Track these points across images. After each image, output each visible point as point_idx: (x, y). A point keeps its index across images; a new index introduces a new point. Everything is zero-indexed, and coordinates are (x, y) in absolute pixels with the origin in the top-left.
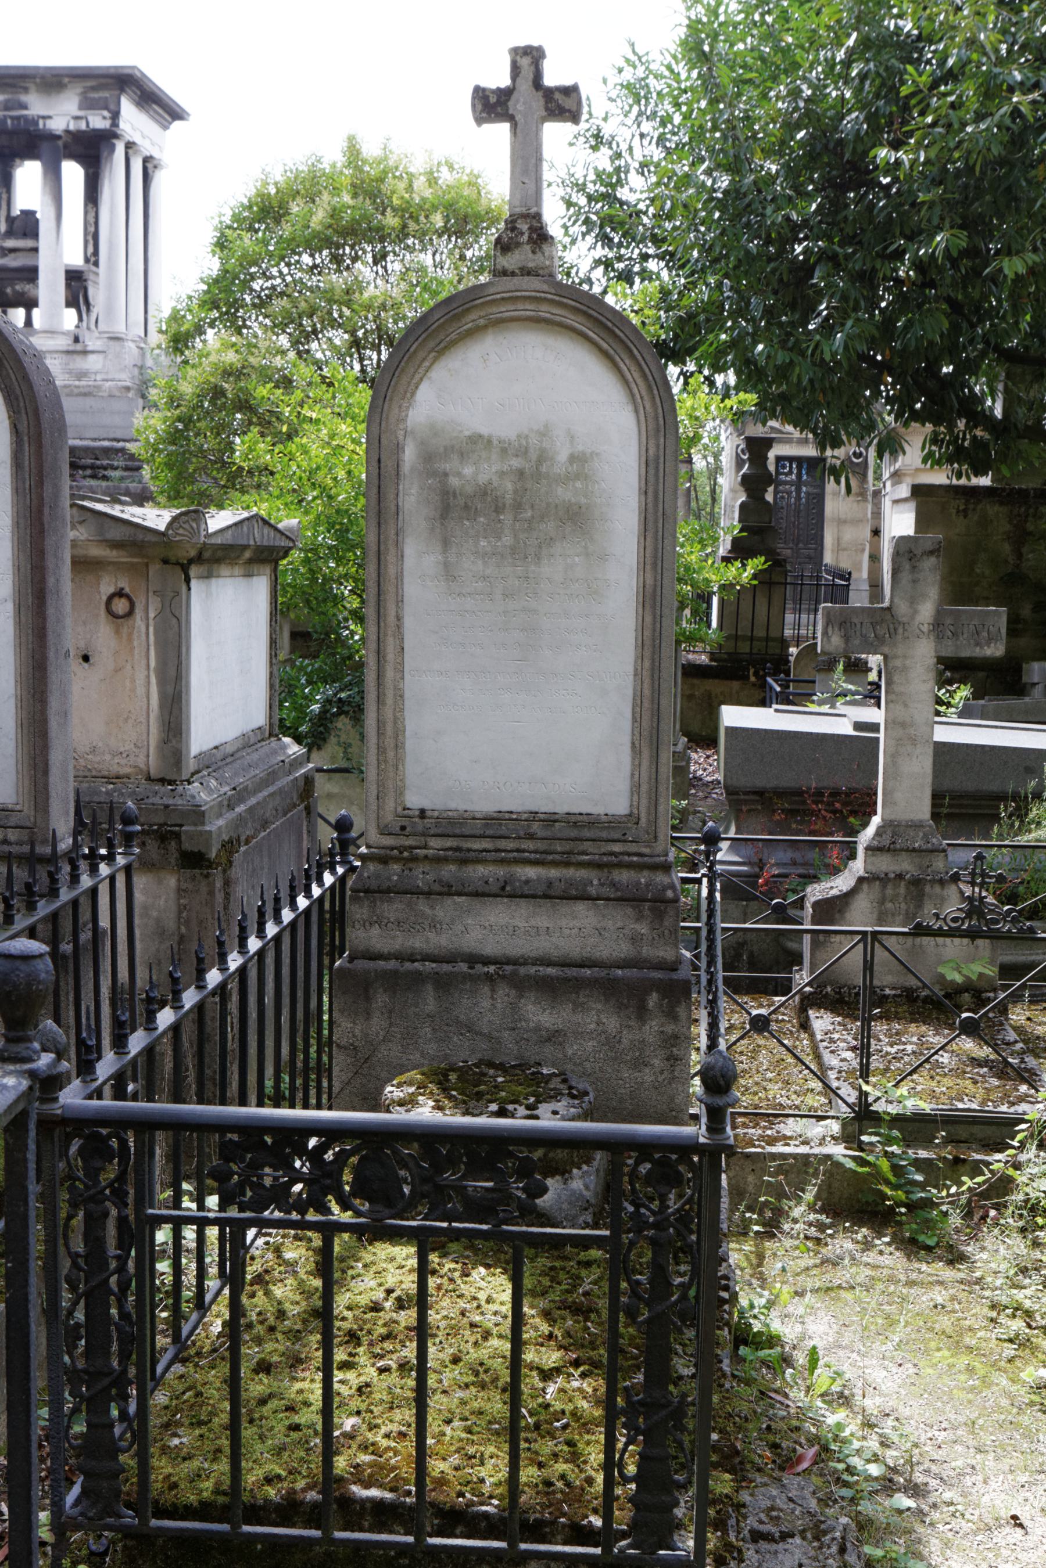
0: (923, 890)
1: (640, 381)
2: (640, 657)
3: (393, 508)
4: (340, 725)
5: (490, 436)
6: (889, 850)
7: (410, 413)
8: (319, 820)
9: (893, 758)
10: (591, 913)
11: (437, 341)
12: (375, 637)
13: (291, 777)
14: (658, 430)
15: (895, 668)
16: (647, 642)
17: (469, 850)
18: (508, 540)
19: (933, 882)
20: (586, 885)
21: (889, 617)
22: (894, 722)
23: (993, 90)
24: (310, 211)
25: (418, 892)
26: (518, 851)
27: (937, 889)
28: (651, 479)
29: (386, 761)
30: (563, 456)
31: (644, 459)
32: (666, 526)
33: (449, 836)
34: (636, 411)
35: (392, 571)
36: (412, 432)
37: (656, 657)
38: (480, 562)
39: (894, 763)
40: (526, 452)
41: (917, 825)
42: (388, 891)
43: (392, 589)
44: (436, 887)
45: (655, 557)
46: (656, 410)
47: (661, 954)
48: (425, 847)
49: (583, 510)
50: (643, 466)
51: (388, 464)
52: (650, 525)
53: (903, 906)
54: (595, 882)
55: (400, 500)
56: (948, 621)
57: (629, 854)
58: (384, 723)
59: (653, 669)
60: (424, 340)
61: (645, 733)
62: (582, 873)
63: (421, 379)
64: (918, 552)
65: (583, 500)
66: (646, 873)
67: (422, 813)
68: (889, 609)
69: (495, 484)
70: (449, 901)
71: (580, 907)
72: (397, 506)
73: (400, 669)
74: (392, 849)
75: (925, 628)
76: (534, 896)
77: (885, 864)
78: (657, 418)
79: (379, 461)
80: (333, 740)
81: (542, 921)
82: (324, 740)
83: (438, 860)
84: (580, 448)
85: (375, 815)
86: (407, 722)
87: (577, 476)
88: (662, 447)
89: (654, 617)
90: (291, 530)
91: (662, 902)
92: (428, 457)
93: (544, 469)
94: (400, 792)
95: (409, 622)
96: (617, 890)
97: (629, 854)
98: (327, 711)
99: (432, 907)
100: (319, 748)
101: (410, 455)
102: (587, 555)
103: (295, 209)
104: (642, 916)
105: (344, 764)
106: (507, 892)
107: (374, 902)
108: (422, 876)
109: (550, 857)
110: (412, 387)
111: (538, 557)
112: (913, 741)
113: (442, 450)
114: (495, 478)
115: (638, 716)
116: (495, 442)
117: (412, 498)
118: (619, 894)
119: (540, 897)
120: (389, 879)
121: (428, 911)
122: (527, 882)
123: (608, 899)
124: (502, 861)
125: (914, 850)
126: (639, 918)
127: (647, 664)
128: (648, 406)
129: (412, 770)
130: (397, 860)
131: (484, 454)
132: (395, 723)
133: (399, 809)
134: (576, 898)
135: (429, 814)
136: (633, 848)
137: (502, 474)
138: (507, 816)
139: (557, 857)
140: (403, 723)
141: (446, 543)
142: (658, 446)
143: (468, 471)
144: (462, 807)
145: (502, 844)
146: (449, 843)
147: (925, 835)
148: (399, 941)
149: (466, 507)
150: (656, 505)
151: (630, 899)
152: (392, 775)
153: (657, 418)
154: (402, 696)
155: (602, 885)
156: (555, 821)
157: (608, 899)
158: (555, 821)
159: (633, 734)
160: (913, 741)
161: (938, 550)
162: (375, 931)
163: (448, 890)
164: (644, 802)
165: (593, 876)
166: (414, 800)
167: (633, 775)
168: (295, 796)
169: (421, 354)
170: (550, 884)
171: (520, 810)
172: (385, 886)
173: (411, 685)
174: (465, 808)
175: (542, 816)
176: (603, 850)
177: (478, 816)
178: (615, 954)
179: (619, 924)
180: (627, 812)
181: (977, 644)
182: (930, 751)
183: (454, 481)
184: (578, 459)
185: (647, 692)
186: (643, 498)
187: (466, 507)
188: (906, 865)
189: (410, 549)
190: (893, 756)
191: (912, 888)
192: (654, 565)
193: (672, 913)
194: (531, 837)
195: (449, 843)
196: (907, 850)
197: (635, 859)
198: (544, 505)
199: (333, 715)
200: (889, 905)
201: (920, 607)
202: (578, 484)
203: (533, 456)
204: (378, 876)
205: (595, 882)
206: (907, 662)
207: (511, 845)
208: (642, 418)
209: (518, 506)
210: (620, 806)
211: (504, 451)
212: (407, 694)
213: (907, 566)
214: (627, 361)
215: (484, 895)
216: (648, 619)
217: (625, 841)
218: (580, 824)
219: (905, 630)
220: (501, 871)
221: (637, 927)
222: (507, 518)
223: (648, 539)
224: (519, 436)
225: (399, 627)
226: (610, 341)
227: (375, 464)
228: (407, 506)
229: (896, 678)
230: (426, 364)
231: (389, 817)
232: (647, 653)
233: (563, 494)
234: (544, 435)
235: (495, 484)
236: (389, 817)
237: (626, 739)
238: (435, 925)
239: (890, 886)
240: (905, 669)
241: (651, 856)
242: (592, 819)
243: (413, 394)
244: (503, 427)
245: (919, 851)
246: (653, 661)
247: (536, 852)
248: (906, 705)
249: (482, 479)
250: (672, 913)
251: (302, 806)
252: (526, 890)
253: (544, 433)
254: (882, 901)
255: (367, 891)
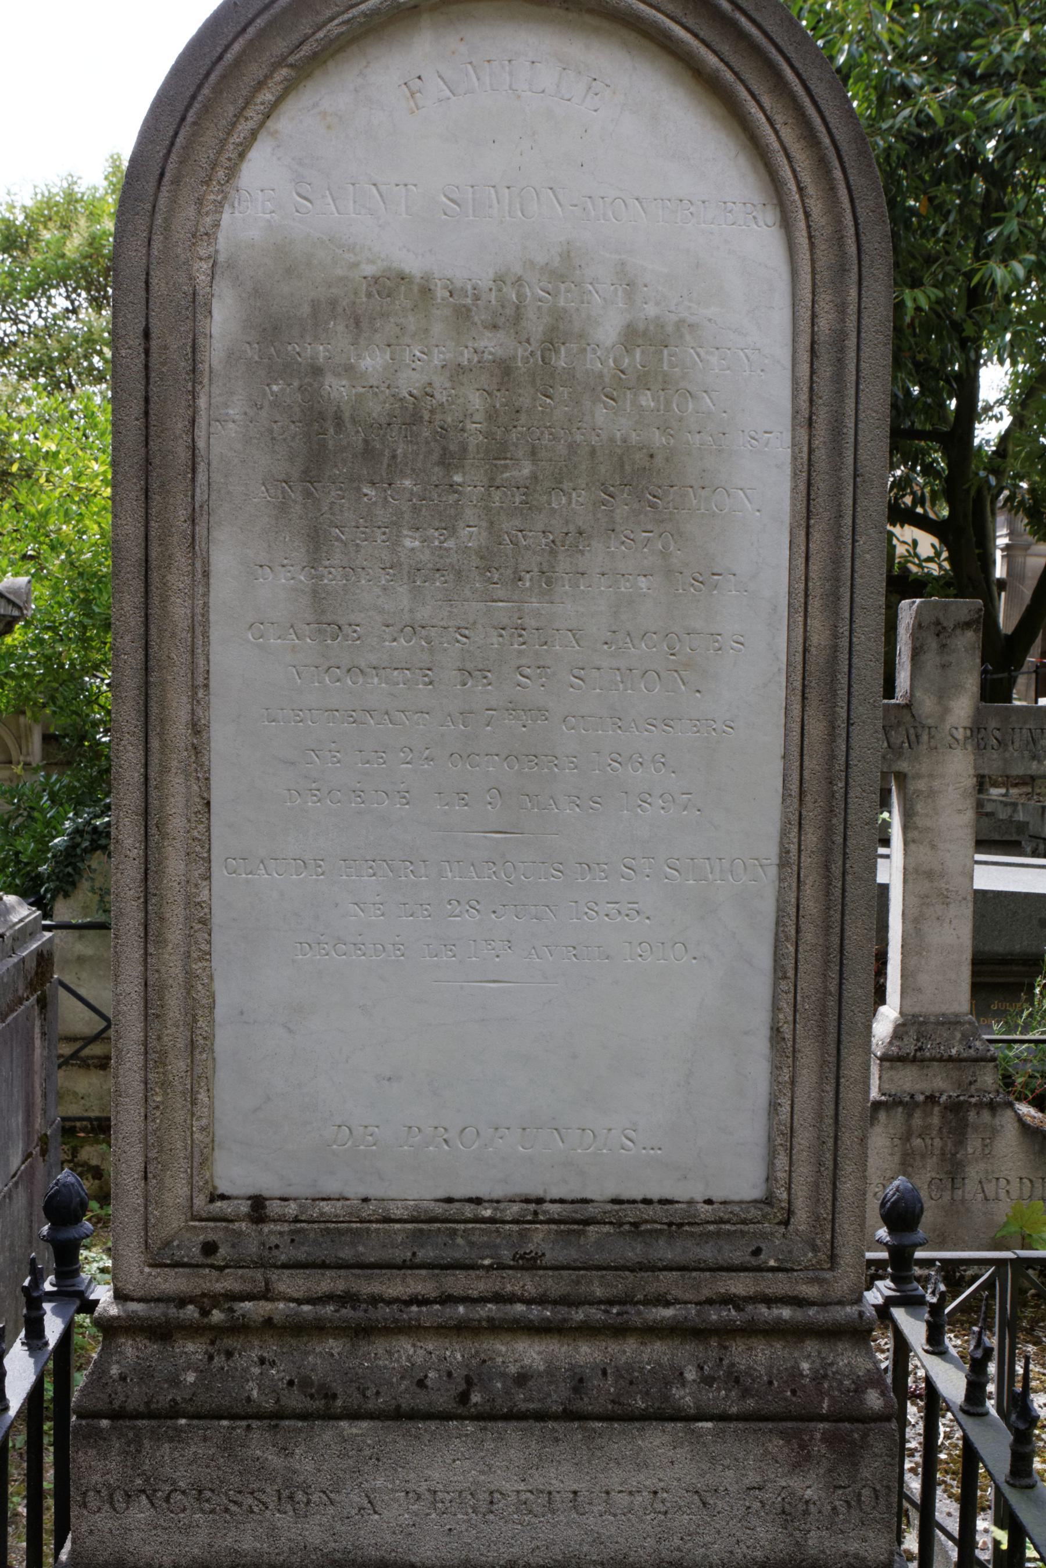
0: (965, 1119)
1: (796, 149)
2: (795, 822)
3: (183, 455)
4: (94, 864)
5: (427, 278)
6: (914, 1060)
7: (226, 217)
8: (62, 992)
9: (913, 921)
10: (682, 1453)
11: (295, 37)
12: (137, 777)
13: (15, 959)
14: (842, 270)
15: (918, 793)
16: (813, 785)
17: (375, 1300)
18: (472, 534)
19: (979, 1105)
20: (667, 1384)
21: (908, 718)
22: (916, 871)
23: (889, 92)
24: (65, 237)
25: (246, 1413)
26: (498, 1298)
27: (986, 1116)
28: (824, 389)
29: (164, 1084)
30: (608, 331)
31: (805, 340)
32: (863, 502)
33: (324, 1266)
34: (786, 224)
35: (179, 611)
36: (230, 265)
37: (837, 821)
38: (403, 590)
39: (918, 931)
40: (518, 317)
41: (951, 1022)
42: (174, 1412)
43: (179, 657)
44: (295, 1400)
45: (835, 579)
46: (837, 220)
47: (853, 1547)
48: (266, 1294)
49: (659, 460)
50: (805, 356)
51: (170, 344)
52: (821, 502)
53: (937, 1142)
54: (691, 1375)
55: (201, 433)
56: (993, 724)
57: (769, 1301)
58: (162, 989)
59: (827, 852)
60: (262, 34)
61: (806, 1006)
62: (656, 1352)
63: (254, 135)
64: (949, 624)
65: (658, 439)
66: (811, 1346)
67: (258, 1202)
68: (908, 706)
69: (441, 397)
70: (327, 1434)
71: (656, 1440)
72: (193, 448)
73: (200, 854)
74: (182, 1302)
75: (960, 734)
76: (540, 1416)
77: (910, 1081)
78: (839, 240)
79: (147, 334)
80: (85, 885)
81: (561, 1477)
82: (74, 884)
83: (298, 1329)
84: (651, 310)
85: (138, 1218)
86: (218, 986)
87: (643, 381)
88: (852, 309)
89: (832, 727)
90: (16, 592)
91: (852, 1419)
92: (270, 328)
93: (561, 362)
94: (201, 1158)
95: (223, 739)
96: (746, 1393)
97: (769, 1301)
98: (78, 845)
99: (285, 1451)
100: (67, 895)
101: (224, 321)
102: (669, 572)
103: (46, 235)
104: (808, 1458)
105: (100, 917)
106: (475, 1406)
107: (138, 1441)
108: (258, 1372)
109: (579, 1315)
110: (230, 152)
111: (547, 577)
112: (945, 898)
113: (306, 310)
114: (440, 382)
115: (789, 964)
116: (440, 293)
117: (232, 429)
118: (751, 1403)
119: (556, 1417)
120: (175, 1382)
121: (274, 1459)
122: (522, 1379)
123: (723, 1417)
124: (462, 1329)
125: (950, 1059)
126: (801, 1462)
127: (812, 838)
128: (816, 208)
129: (230, 1100)
130: (193, 1330)
131: (412, 322)
132: (189, 988)
133: (200, 1201)
134: (644, 1417)
135: (274, 1208)
136: (778, 1285)
137: (458, 372)
138: (469, 1210)
139: (596, 1314)
140: (209, 987)
141: (317, 542)
142: (841, 309)
143: (372, 362)
144: (356, 1190)
145: (458, 1283)
146: (327, 1283)
147: (965, 1037)
148: (202, 1537)
149: (368, 453)
150: (836, 451)
151: (783, 1416)
152: (180, 1116)
153: (839, 240)
154: (205, 922)
155: (707, 1381)
156: (587, 1222)
157: (723, 1417)
158: (587, 1222)
159: (776, 1008)
160: (945, 898)
161: (977, 621)
162: (140, 1513)
163: (324, 1406)
164: (804, 1171)
165: (686, 1358)
166: (237, 1174)
167: (774, 1106)
168: (21, 986)
169: (255, 71)
170: (579, 1383)
171: (498, 1193)
172: (163, 1400)
173: (228, 892)
174: (363, 1191)
175: (554, 1209)
176: (706, 1293)
177: (397, 1212)
178: (739, 1551)
179: (753, 1478)
180: (757, 1192)
181: (1034, 757)
182: (967, 911)
183: (337, 389)
184: (648, 338)
185: (811, 907)
186: (803, 435)
187: (368, 453)
188: (938, 1081)
189: (228, 554)
190: (916, 920)
191: (950, 1116)
192: (833, 597)
193: (879, 1447)
194: (530, 1263)
195: (327, 1283)
196: (941, 1060)
197: (786, 1313)
198: (562, 449)
199: (85, 850)
200: (917, 1142)
201: (952, 704)
202: (646, 400)
203: (535, 326)
204: (145, 1374)
205: (691, 1375)
206: (936, 784)
207: (479, 1285)
208: (802, 239)
209: (498, 453)
210: (741, 1180)
211: (462, 314)
212: (219, 917)
213: (933, 644)
214: (766, 100)
215: (414, 1415)
216: (816, 729)
217: (759, 1269)
218: (647, 1226)
219: (931, 737)
220: (457, 1353)
221: (795, 1483)
222: (469, 479)
223: (816, 536)
224: (499, 279)
225: (198, 750)
226: (725, 48)
227: (136, 341)
228: (217, 450)
229: (919, 807)
230: (267, 96)
231: (173, 1221)
232: (813, 812)
233: (608, 422)
234: (562, 278)
235: (441, 397)
236: (173, 1221)
237: (758, 1020)
238: (291, 1495)
239: (918, 1114)
240: (932, 794)
241: (823, 1304)
242: (676, 1212)
243: (233, 172)
244: (459, 258)
245: (957, 1060)
246: (829, 831)
247: (542, 1300)
248: (933, 847)
249: (409, 382)
250: (879, 1447)
251: (33, 999)
252: (521, 1400)
253: (564, 270)
254: (907, 1137)
255: (116, 1415)
